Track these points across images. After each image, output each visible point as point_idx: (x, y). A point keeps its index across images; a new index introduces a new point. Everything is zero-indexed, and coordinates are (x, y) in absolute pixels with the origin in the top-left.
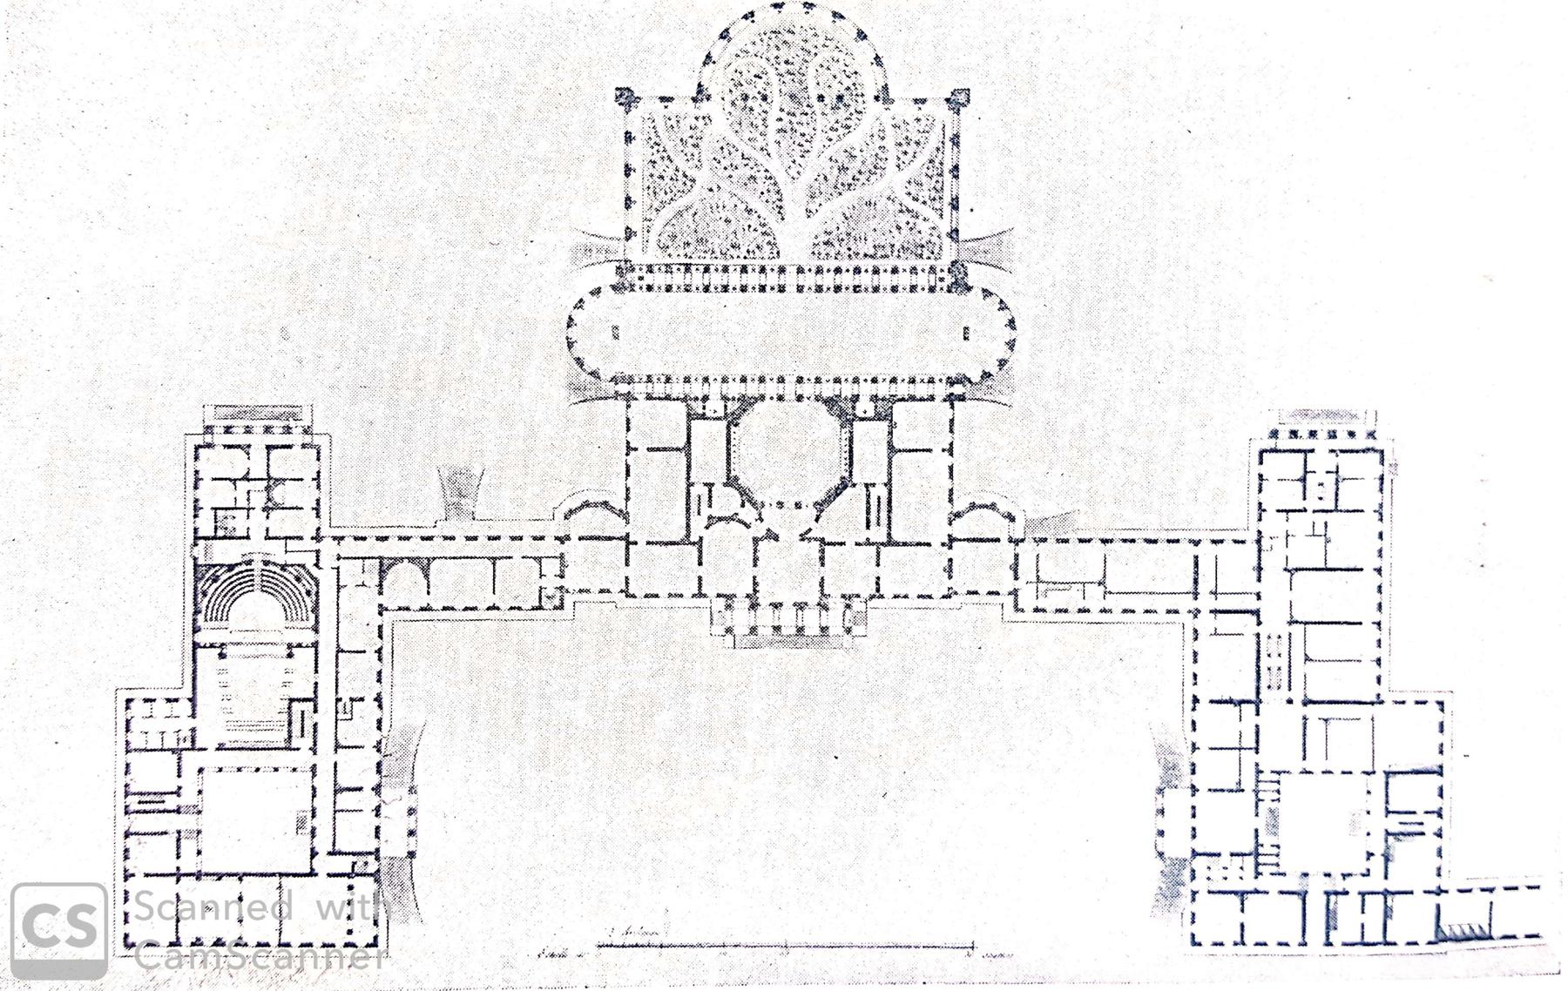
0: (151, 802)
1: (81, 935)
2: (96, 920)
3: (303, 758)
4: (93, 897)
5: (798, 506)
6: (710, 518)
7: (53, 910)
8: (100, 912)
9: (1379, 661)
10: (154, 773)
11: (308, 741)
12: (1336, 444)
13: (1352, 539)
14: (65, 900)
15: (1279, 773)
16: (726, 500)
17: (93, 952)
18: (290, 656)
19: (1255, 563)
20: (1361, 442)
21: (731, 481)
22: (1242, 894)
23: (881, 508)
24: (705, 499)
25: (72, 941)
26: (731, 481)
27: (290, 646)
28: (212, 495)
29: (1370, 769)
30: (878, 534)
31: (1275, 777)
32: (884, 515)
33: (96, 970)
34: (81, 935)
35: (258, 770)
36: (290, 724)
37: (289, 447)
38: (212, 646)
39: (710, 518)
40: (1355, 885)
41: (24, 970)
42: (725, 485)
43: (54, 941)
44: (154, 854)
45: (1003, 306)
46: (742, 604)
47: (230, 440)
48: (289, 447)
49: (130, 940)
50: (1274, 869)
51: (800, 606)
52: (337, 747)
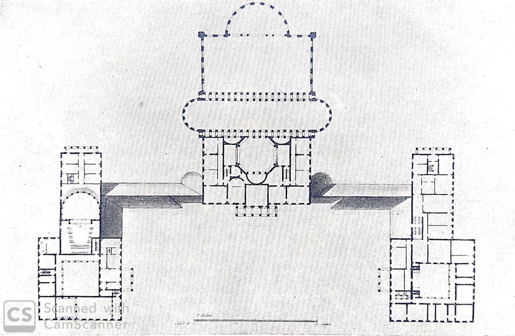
0: (46, 272)
1: (27, 317)
2: (31, 312)
3: (96, 258)
4: (30, 305)
5: (254, 173)
6: (231, 177)
7: (17, 309)
8: (33, 310)
9: (453, 226)
10: (47, 262)
11: (98, 252)
12: (438, 152)
13: (443, 184)
14: (22, 306)
15: (419, 263)
16: (236, 172)
17: (30, 323)
18: (92, 223)
19: (62, 210)
20: (446, 151)
21: (237, 165)
22: (407, 304)
23: (286, 174)
24: (229, 171)
25: (24, 320)
26: (237, 165)
27: (92, 220)
28: (67, 169)
29: (450, 262)
30: (287, 182)
31: (417, 265)
32: (288, 175)
33: (32, 329)
34: (27, 317)
35: (87, 262)
36: (92, 247)
37: (91, 153)
38: (66, 220)
39: (231, 177)
40: (443, 302)
41: (8, 329)
42: (236, 166)
43: (18, 319)
44: (47, 290)
45: (327, 106)
46: (241, 206)
47: (72, 151)
48: (91, 153)
49: (41, 318)
50: (417, 296)
51: (260, 207)
52: (436, 304)
